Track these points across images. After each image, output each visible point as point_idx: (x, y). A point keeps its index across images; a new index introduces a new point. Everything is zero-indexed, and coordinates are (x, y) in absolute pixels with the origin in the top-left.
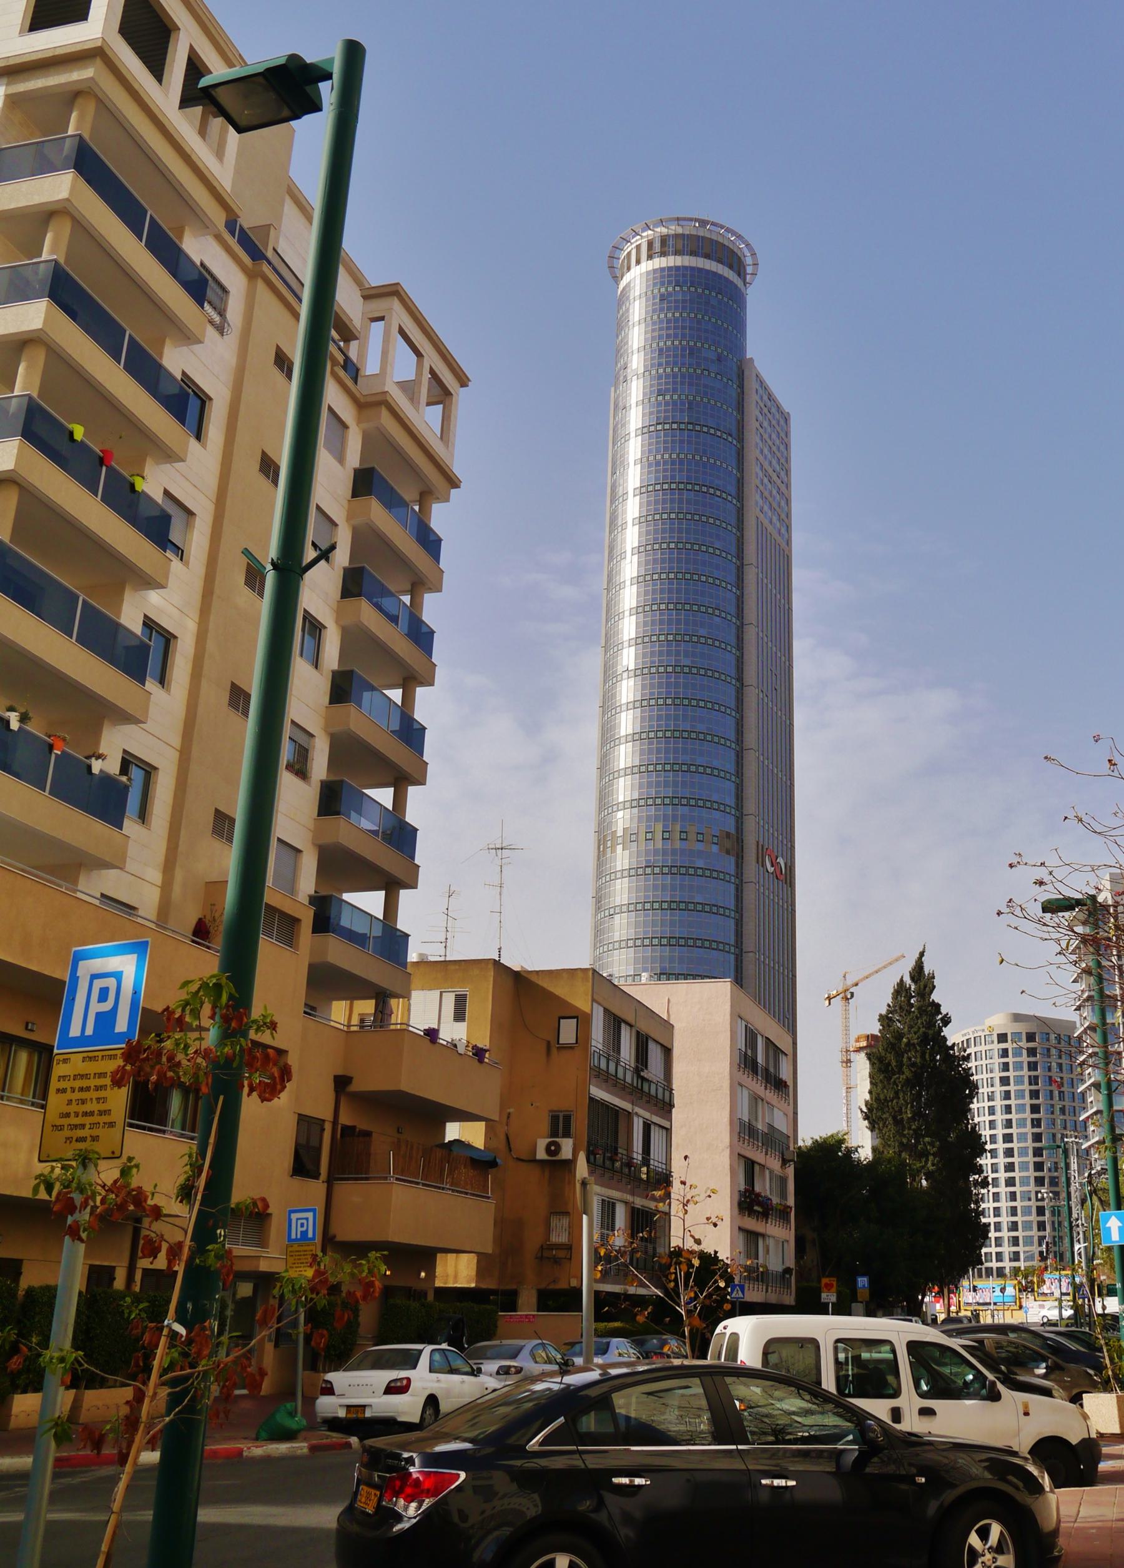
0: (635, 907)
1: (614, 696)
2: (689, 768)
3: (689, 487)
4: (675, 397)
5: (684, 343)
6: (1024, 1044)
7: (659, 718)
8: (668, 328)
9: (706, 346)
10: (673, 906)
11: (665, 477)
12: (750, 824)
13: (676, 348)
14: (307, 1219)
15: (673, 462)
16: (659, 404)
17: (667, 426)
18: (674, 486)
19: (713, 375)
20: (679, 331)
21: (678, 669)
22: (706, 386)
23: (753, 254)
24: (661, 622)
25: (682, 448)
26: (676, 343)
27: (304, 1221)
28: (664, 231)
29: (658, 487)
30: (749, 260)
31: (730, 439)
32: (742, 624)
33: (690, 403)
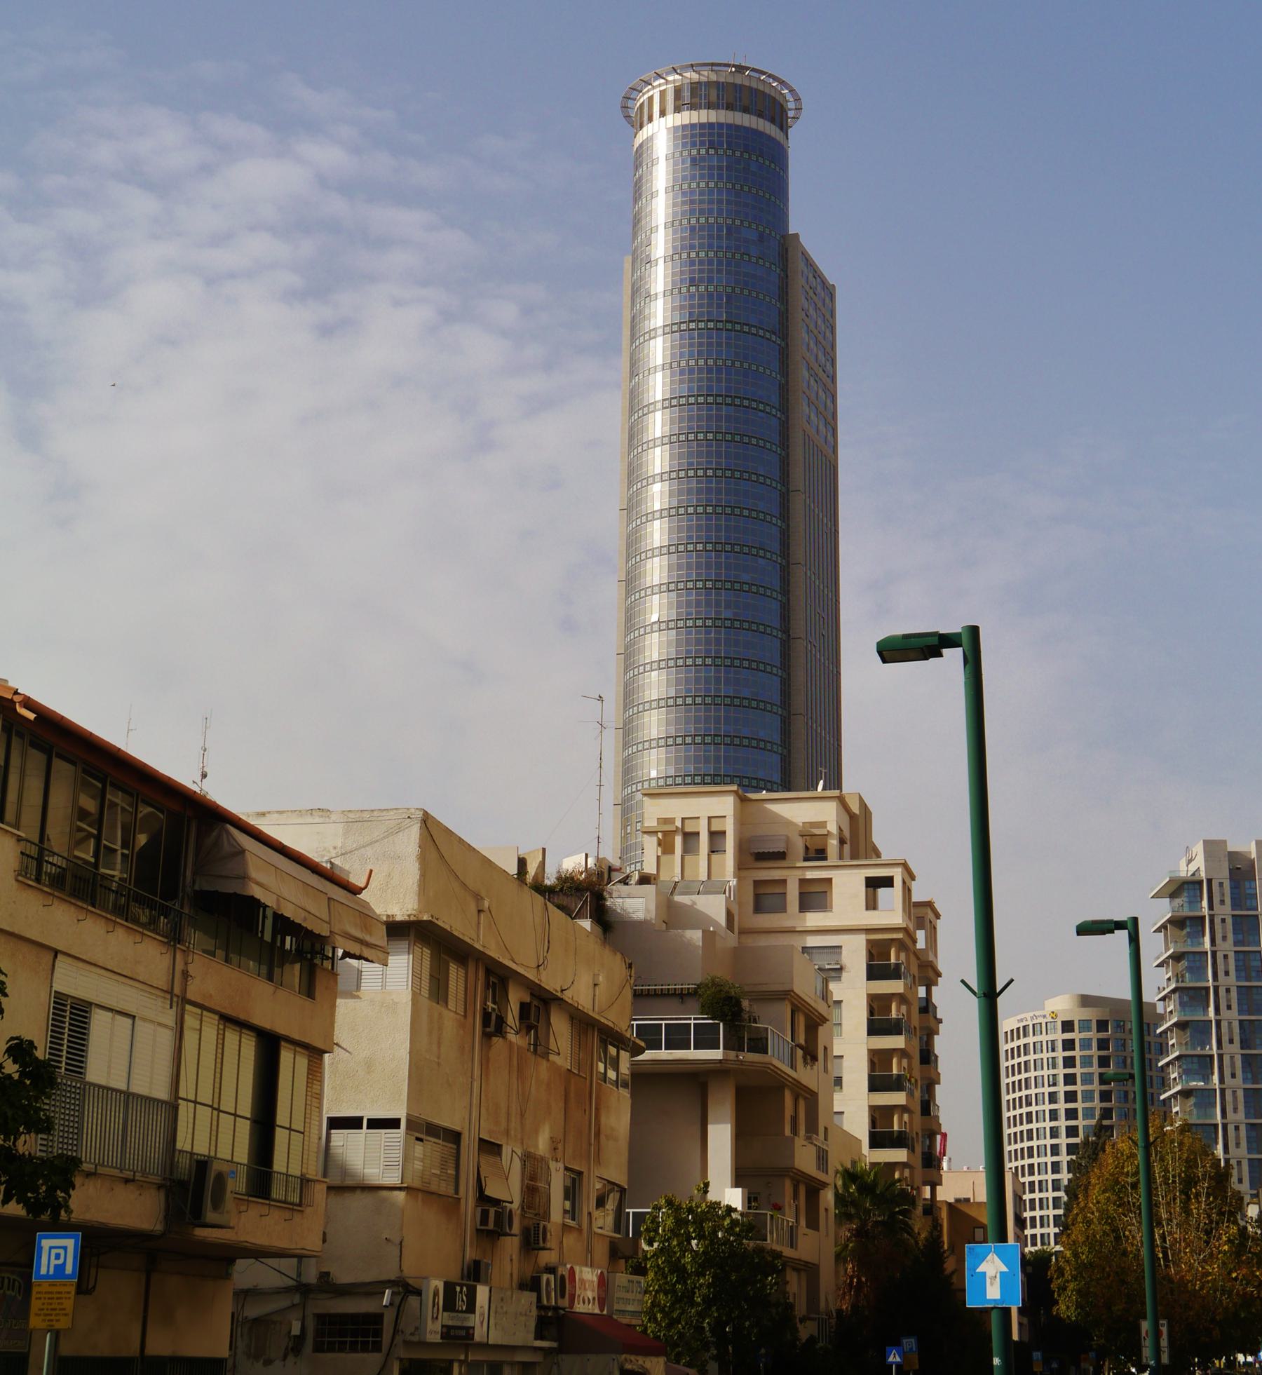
0: (668, 742)
1: (640, 466)
2: (733, 586)
3: (729, 400)
4: (711, 289)
5: (721, 220)
6: (1093, 1034)
7: (697, 680)
8: (701, 202)
9: (746, 224)
11: (699, 388)
13: (710, 226)
14: (65, 1248)
16: (692, 296)
17: (702, 325)
18: (710, 400)
19: (754, 260)
23: (798, 100)
24: (698, 566)
25: (719, 353)
26: (711, 220)
27: (62, 1251)
28: (695, 77)
29: (692, 400)
30: (791, 105)
32: (788, 562)
33: (729, 229)
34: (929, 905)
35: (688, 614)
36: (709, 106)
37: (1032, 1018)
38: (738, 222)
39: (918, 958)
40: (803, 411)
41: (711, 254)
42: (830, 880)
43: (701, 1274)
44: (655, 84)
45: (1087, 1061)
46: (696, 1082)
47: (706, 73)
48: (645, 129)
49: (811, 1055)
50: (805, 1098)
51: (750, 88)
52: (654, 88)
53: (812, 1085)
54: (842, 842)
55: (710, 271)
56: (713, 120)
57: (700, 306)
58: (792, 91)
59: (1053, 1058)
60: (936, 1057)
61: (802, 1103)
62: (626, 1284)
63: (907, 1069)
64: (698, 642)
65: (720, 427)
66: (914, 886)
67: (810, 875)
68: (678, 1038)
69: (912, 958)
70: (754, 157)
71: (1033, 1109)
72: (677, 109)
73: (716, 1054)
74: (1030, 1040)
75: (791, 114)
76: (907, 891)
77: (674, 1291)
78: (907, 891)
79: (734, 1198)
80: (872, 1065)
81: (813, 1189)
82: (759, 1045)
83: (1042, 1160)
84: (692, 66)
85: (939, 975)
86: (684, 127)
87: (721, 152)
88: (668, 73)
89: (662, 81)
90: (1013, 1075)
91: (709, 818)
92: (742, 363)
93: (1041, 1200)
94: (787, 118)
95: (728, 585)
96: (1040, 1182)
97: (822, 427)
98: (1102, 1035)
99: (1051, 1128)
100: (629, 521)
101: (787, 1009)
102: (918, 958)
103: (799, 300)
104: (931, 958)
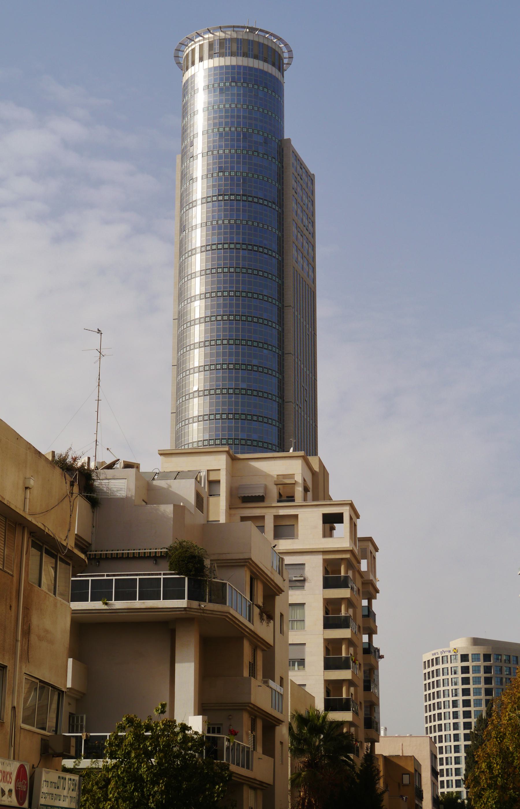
3: (244, 247)
4: (233, 174)
6: (481, 663)
9: (256, 132)
10: (237, 391)
16: (220, 179)
17: (226, 198)
18: (232, 246)
19: (261, 155)
20: (235, 120)
23: (290, 51)
26: (233, 129)
28: (222, 35)
29: (220, 246)
30: (286, 55)
31: (274, 206)
32: (283, 353)
34: (370, 540)
36: (232, 54)
37: (441, 653)
38: (250, 131)
39: (362, 577)
40: (293, 256)
41: (233, 151)
42: (296, 517)
43: (154, 783)
45: (477, 681)
46: (165, 629)
47: (229, 33)
48: (189, 70)
49: (268, 614)
50: (263, 650)
51: (259, 43)
52: (195, 43)
53: (269, 640)
54: (306, 490)
55: (232, 162)
56: (234, 63)
58: (286, 45)
59: (456, 689)
60: (289, 140)
61: (260, 655)
62: (56, 780)
63: (355, 658)
66: (359, 522)
67: (282, 512)
68: (149, 590)
69: (357, 575)
70: (261, 88)
71: (442, 711)
72: (211, 57)
73: (182, 603)
74: (440, 666)
75: (286, 61)
76: (353, 527)
77: (131, 798)
78: (353, 527)
79: (196, 724)
80: (327, 650)
81: (270, 724)
82: (219, 594)
83: (448, 744)
85: (377, 591)
86: (215, 68)
87: (239, 84)
88: (205, 33)
89: (201, 38)
90: (429, 689)
91: (208, 470)
92: (253, 222)
93: (447, 770)
94: (283, 64)
95: (244, 367)
96: (447, 758)
97: (305, 266)
98: (487, 664)
99: (456, 769)
100: (179, 326)
101: (245, 575)
102: (362, 577)
103: (291, 182)
104: (371, 577)
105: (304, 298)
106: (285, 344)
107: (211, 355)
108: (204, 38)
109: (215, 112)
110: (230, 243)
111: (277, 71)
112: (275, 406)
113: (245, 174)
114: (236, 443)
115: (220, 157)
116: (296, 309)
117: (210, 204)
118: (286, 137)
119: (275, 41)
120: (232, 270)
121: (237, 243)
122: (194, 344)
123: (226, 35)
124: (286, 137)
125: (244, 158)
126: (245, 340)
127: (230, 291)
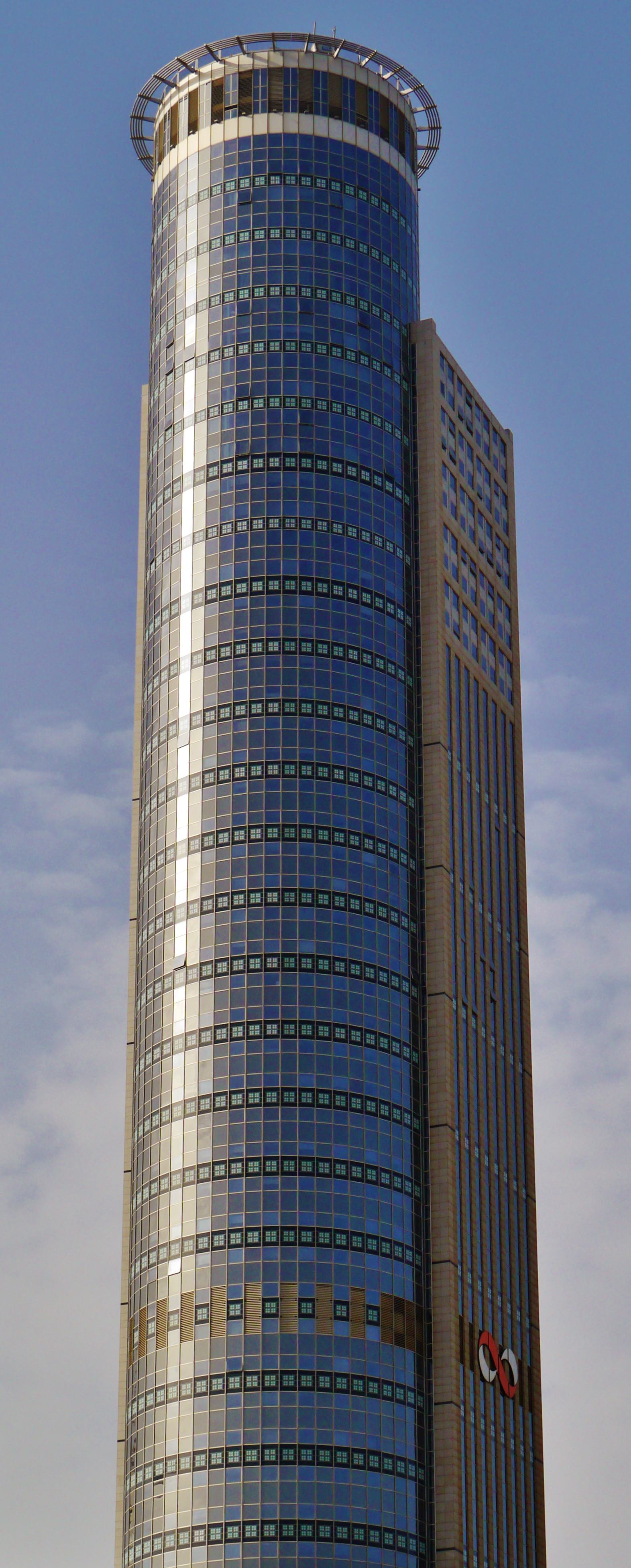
3: (307, 586)
4: (275, 402)
8: (257, 262)
9: (336, 297)
10: (291, 963)
12: (446, 1286)
15: (272, 536)
16: (241, 418)
17: (259, 463)
18: (274, 585)
19: (351, 356)
20: (281, 268)
21: (290, 963)
22: (337, 379)
23: (431, 108)
26: (275, 291)
28: (246, 62)
30: (421, 120)
35: (234, 949)
38: (322, 294)
41: (275, 346)
44: (181, 84)
47: (264, 55)
51: (343, 80)
52: (179, 89)
57: (256, 432)
58: (418, 89)
64: (253, 997)
65: (292, 1079)
70: (350, 190)
75: (422, 139)
84: (239, 41)
86: (228, 145)
87: (291, 180)
89: (193, 76)
100: (134, 1190)
105: (486, 863)
106: (423, 690)
107: (220, 869)
108: (199, 73)
109: (227, 251)
110: (269, 579)
111: (395, 153)
112: (402, 1004)
113: (306, 403)
114: (285, 1384)
115: (242, 362)
116: (458, 877)
117: (206, 1257)
118: (423, 317)
119: (386, 76)
120: (273, 897)
121: (286, 578)
122: (170, 1175)
123: (257, 62)
124: (423, 317)
125: (306, 361)
126: (311, 1023)
127: (268, 701)
